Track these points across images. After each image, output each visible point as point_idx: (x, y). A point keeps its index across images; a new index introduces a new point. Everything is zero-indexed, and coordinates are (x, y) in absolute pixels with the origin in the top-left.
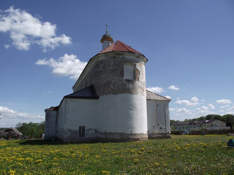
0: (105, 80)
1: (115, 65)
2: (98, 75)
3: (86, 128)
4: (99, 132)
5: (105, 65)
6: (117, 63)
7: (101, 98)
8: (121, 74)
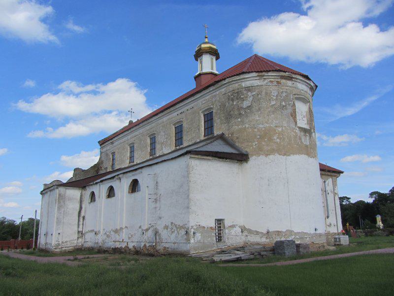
0: (261, 126)
1: (279, 97)
2: (240, 114)
3: (227, 223)
4: (250, 231)
5: (260, 96)
6: (284, 94)
7: (253, 160)
8: (292, 116)
